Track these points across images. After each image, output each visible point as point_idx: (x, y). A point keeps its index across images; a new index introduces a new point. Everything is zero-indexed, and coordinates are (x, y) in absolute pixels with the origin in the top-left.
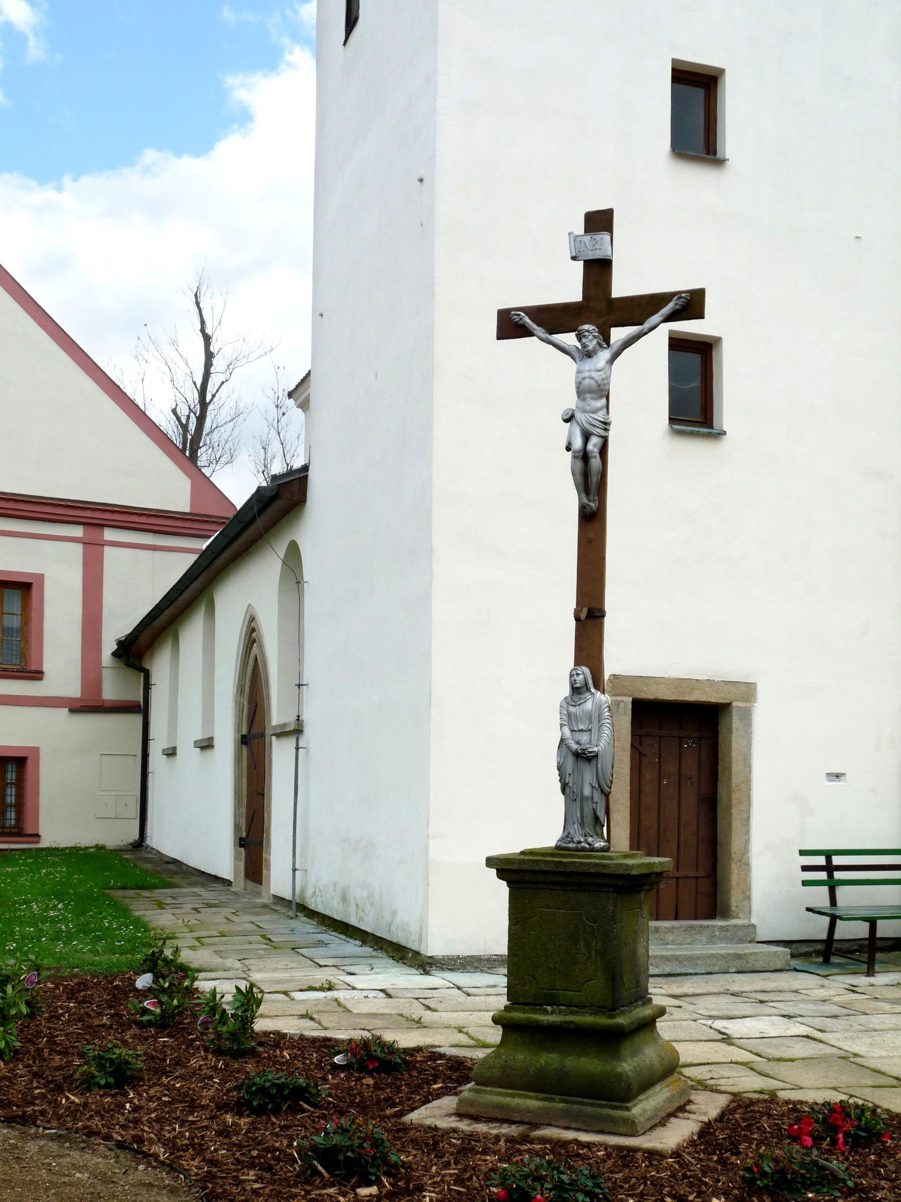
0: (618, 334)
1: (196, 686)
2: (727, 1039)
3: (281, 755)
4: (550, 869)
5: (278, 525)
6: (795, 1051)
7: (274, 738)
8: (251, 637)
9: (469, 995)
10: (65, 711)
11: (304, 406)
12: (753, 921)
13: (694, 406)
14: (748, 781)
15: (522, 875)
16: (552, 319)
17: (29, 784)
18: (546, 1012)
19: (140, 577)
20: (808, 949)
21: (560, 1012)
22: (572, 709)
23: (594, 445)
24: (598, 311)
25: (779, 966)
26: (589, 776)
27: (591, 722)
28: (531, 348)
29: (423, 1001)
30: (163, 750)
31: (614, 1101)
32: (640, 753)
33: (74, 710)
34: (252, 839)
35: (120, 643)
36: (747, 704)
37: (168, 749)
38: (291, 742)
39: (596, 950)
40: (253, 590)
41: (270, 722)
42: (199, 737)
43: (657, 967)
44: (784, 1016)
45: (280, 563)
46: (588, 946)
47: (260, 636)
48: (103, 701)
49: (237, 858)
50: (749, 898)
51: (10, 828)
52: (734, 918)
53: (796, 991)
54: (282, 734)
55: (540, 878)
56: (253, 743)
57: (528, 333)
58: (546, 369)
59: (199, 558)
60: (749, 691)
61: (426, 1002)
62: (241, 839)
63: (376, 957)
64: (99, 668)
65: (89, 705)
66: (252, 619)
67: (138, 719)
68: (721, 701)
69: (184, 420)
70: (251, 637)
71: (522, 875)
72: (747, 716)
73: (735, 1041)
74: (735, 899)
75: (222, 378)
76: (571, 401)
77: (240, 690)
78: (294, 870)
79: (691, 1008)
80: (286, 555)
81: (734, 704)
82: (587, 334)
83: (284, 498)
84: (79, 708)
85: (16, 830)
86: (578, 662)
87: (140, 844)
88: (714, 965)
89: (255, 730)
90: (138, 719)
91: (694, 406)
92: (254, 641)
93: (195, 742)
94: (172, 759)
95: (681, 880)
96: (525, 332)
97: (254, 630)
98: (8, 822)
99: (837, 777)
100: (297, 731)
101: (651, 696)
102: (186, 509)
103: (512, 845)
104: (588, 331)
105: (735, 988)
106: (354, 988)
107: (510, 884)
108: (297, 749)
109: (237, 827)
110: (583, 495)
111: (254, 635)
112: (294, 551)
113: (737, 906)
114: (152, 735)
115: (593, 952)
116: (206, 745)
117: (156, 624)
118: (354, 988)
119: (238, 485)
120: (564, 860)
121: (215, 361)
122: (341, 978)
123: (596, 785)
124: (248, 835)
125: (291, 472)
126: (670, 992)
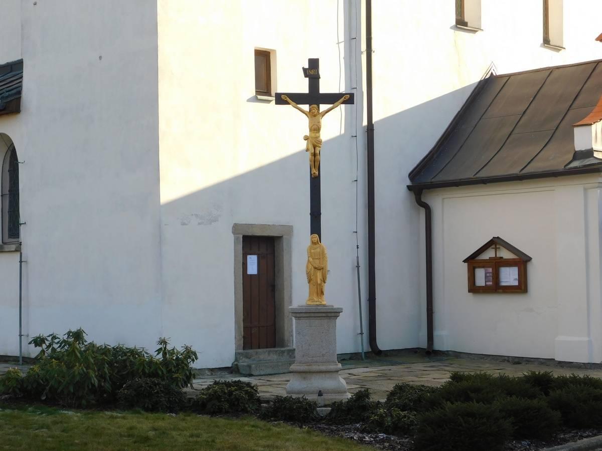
14: (290, 276)
15: (36, 346)
16: (297, 99)
22: (312, 251)
26: (319, 275)
43: (264, 371)
57: (288, 104)
59: (476, 257)
71: (36, 346)
76: (307, 133)
78: (21, 336)
81: (284, 237)
96: (287, 103)
108: (21, 262)
120: (319, 308)
123: (322, 279)
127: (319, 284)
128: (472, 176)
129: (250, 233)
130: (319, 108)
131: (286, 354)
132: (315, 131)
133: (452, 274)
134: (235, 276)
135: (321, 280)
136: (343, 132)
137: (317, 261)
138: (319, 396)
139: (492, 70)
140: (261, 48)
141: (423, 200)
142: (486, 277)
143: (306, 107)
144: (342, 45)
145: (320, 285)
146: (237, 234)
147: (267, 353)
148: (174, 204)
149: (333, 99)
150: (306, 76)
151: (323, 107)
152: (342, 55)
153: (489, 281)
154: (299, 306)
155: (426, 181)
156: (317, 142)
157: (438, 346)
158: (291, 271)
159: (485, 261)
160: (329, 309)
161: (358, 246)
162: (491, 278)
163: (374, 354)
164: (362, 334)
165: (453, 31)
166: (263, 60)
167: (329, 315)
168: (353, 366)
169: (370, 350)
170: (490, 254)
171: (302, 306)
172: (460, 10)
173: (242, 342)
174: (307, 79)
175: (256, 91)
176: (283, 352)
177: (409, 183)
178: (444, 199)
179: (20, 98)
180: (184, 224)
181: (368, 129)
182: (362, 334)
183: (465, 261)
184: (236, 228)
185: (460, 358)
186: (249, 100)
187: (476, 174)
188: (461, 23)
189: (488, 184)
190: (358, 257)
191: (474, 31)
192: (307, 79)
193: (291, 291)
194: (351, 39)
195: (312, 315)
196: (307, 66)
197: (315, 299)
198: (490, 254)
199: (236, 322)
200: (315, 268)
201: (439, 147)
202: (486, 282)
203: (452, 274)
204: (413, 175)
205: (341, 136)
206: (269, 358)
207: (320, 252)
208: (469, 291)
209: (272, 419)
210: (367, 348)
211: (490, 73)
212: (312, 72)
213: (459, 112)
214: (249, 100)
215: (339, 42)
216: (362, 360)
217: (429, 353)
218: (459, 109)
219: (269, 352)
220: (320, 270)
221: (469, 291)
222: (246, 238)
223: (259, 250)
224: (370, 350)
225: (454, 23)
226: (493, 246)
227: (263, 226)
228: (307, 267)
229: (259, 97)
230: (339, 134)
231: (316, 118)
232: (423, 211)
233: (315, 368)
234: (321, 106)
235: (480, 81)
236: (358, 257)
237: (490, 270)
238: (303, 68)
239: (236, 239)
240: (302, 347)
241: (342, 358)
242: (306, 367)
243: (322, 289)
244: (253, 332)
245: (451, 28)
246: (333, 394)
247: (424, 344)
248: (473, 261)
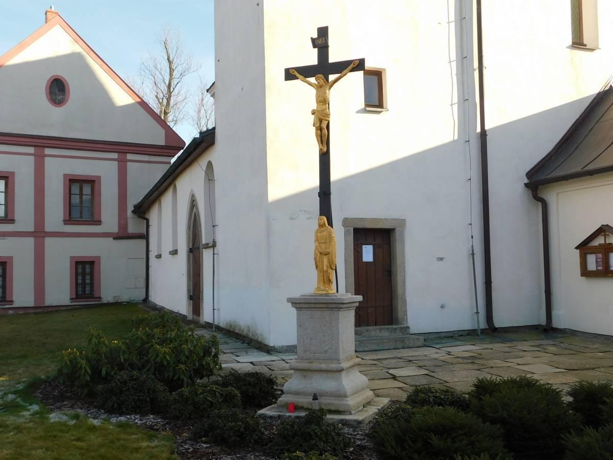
0: (332, 77)
1: (168, 224)
2: (394, 378)
3: (207, 255)
5: (203, 154)
7: (204, 249)
8: (193, 204)
9: (287, 363)
10: (112, 238)
11: (213, 96)
12: (409, 326)
13: (375, 99)
14: (404, 263)
15: (301, 305)
16: (305, 72)
17: (96, 274)
19: (144, 174)
20: (432, 337)
22: (319, 234)
23: (324, 125)
24: (324, 70)
25: (419, 345)
27: (326, 239)
28: (298, 84)
29: (268, 366)
30: (170, 252)
32: (358, 252)
33: (114, 239)
34: (195, 296)
35: (135, 207)
37: (158, 255)
38: (211, 250)
40: (191, 182)
41: (202, 242)
42: (156, 254)
44: (419, 367)
45: (204, 173)
47: (196, 203)
48: (129, 234)
49: (189, 305)
50: (406, 315)
51: (88, 295)
53: (426, 356)
54: (207, 246)
55: (312, 306)
56: (195, 252)
58: (304, 92)
60: (403, 222)
61: (269, 367)
62: (191, 296)
63: (249, 348)
64: (126, 219)
65: (122, 235)
66: (193, 196)
67: (144, 242)
69: (161, 101)
70: (193, 204)
71: (301, 305)
72: (402, 233)
73: (397, 378)
74: (400, 314)
75: (178, 80)
77: (189, 228)
78: (214, 310)
79: (381, 365)
80: (206, 168)
83: (206, 140)
84: (117, 237)
85: (90, 296)
86: (321, 214)
87: (146, 299)
89: (195, 246)
90: (144, 242)
91: (375, 99)
92: (194, 206)
93: (170, 252)
94: (159, 259)
96: (295, 78)
97: (194, 201)
98: (87, 292)
99: (441, 259)
100: (214, 246)
101: (361, 227)
102: (163, 144)
103: (297, 294)
105: (399, 356)
106: (239, 362)
108: (214, 254)
109: (189, 290)
110: (321, 145)
111: (194, 203)
112: (210, 164)
114: (151, 248)
116: (174, 252)
117: (152, 197)
118: (239, 362)
119: (187, 133)
121: (174, 73)
122: (233, 358)
123: (328, 265)
124: (193, 294)
125: (208, 130)
126: (373, 358)
127: (325, 271)
128: (580, 170)
129: (360, 225)
131: (398, 331)
132: (321, 104)
133: (566, 260)
135: (328, 267)
136: (456, 137)
137: (323, 246)
138: (313, 399)
139: (611, 83)
140: (372, 68)
141: (540, 195)
142: (597, 262)
144: (454, 64)
145: (327, 271)
146: (346, 227)
147: (378, 331)
148: (283, 203)
150: (314, 47)
152: (454, 72)
153: (600, 266)
154: (301, 296)
155: (540, 180)
156: (323, 115)
157: (558, 323)
158: (404, 258)
159: (595, 247)
160: (332, 299)
162: (601, 263)
163: (491, 331)
164: (477, 313)
165: (569, 50)
167: (331, 306)
168: (459, 343)
169: (488, 327)
170: (600, 241)
171: (304, 296)
172: (579, 35)
174: (316, 49)
176: (395, 329)
177: (526, 181)
178: (558, 193)
179: (215, 132)
180: (292, 219)
181: (481, 135)
182: (477, 313)
183: (577, 248)
185: (577, 336)
186: (358, 112)
187: (584, 168)
188: (578, 43)
189: (595, 175)
190: (472, 246)
191: (592, 50)
192: (316, 49)
193: (405, 276)
194: (463, 58)
195: (312, 306)
196: (315, 36)
197: (322, 287)
198: (600, 241)
200: (321, 253)
201: (557, 150)
202: (597, 267)
203: (566, 260)
204: (530, 174)
205: (454, 141)
206: (381, 335)
207: (326, 236)
208: (582, 276)
209: (203, 439)
210: (483, 325)
211: (609, 85)
212: (320, 42)
213: (578, 120)
214: (358, 112)
215: (451, 60)
216: (478, 335)
217: (547, 331)
218: (577, 117)
219: (380, 330)
220: (326, 255)
221: (582, 276)
223: (375, 241)
224: (488, 327)
225: (571, 43)
226: (603, 234)
228: (315, 252)
229: (368, 109)
230: (452, 140)
231: (323, 88)
232: (540, 204)
233: (315, 366)
235: (599, 94)
236: (472, 246)
237: (600, 256)
238: (312, 38)
240: (304, 341)
241: (459, 334)
242: (307, 364)
243: (329, 277)
244: (369, 311)
245: (568, 47)
246: (332, 398)
247: (543, 322)
248: (584, 247)
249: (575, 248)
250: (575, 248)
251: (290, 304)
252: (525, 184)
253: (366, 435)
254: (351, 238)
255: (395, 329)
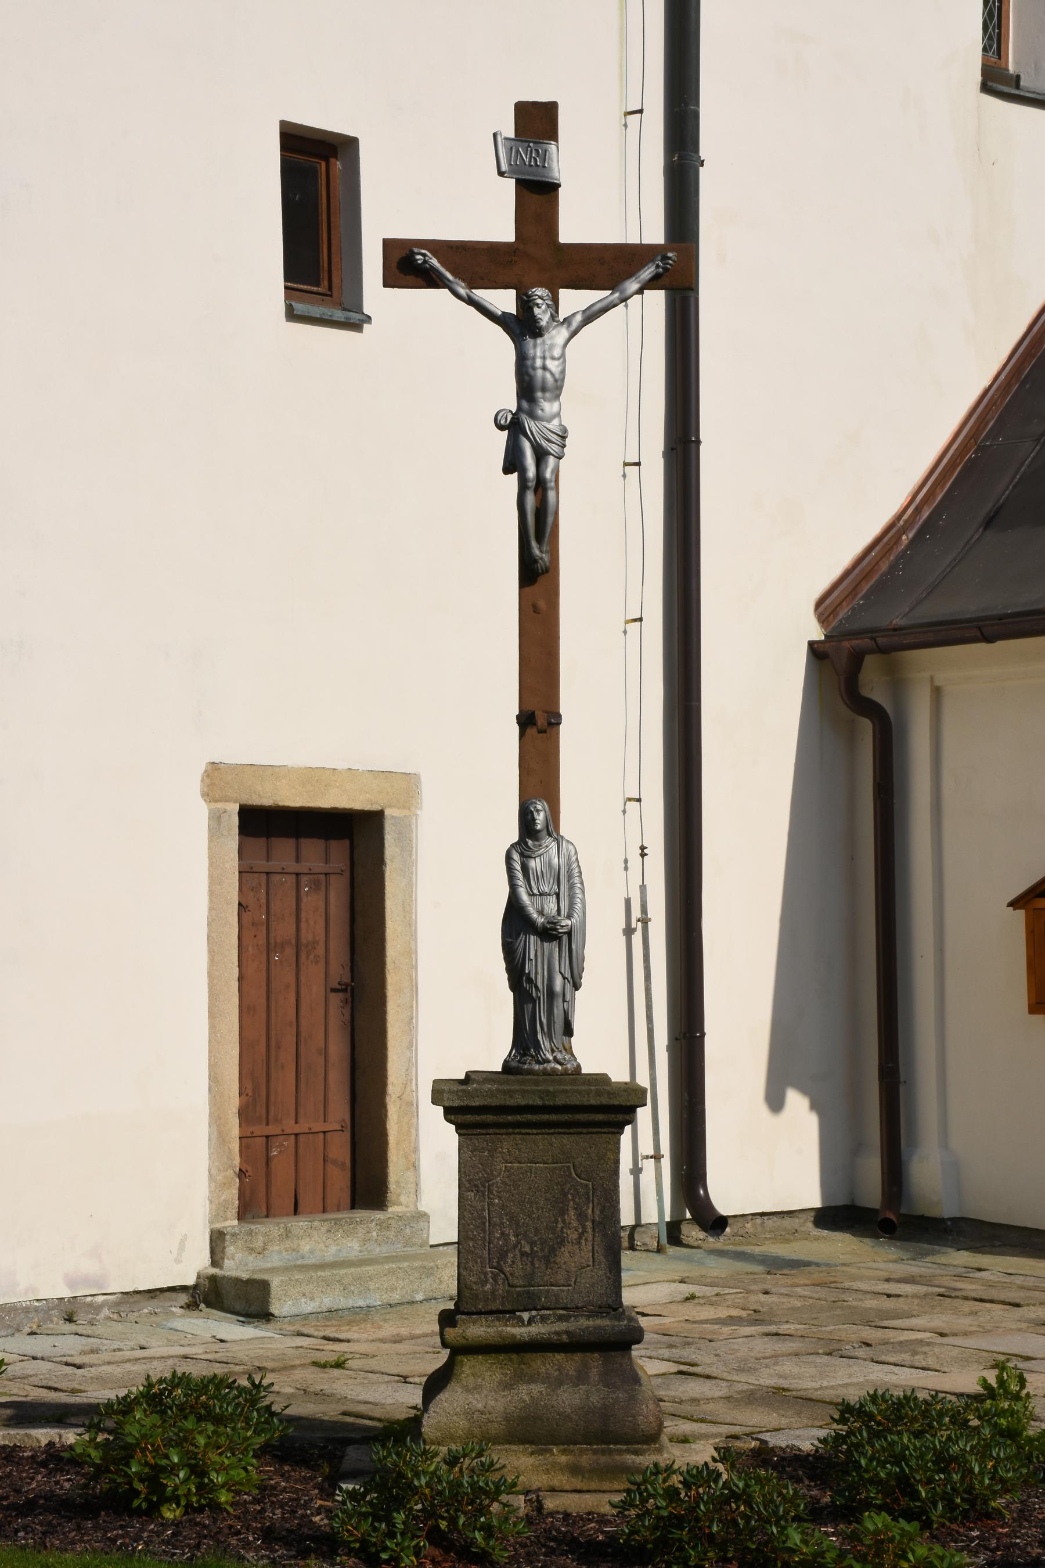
4: (531, 1102)
6: (785, 1367)
12: (423, 1207)
18: (521, 1322)
21: (544, 1319)
31: (638, 1443)
36: (405, 812)
39: (593, 1222)
43: (312, 1299)
46: (581, 1216)
52: (395, 1204)
60: (408, 785)
68: (368, 807)
81: (387, 812)
82: (539, 301)
88: (393, 1289)
95: (302, 1138)
96: (429, 279)
101: (267, 802)
104: (541, 298)
107: (459, 1127)
113: (398, 1182)
115: (589, 1224)
130: (555, 300)
134: (211, 952)
143: (504, 301)
146: (216, 801)
149: (607, 268)
151: (574, 300)
161: (643, 848)
166: (316, 170)
173: (236, 1192)
175: (286, 288)
183: (1014, 904)
184: (284, 124)
196: (509, 130)
199: (216, 1119)
222: (261, 824)
227: (312, 775)
234: (564, 294)
239: (216, 818)
249: (1010, 905)
250: (1010, 905)
251: (440, 1110)
252: (811, 644)
253: (921, 1529)
254: (232, 841)
255: (337, 1219)
